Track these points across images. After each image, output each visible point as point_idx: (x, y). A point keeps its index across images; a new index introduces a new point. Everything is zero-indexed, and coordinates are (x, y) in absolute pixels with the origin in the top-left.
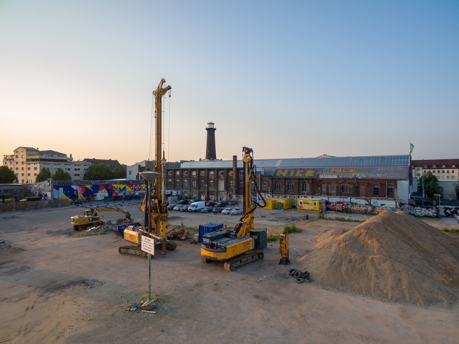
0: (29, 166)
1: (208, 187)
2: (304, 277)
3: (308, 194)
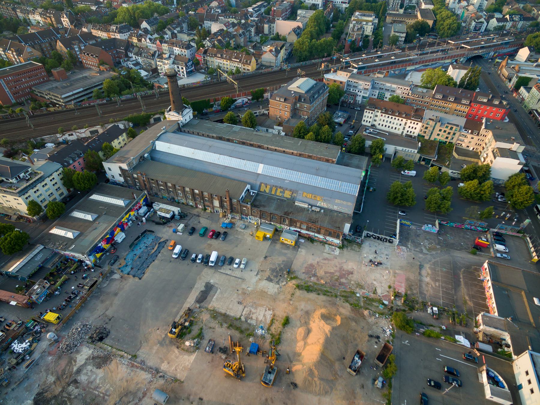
2: (295, 385)
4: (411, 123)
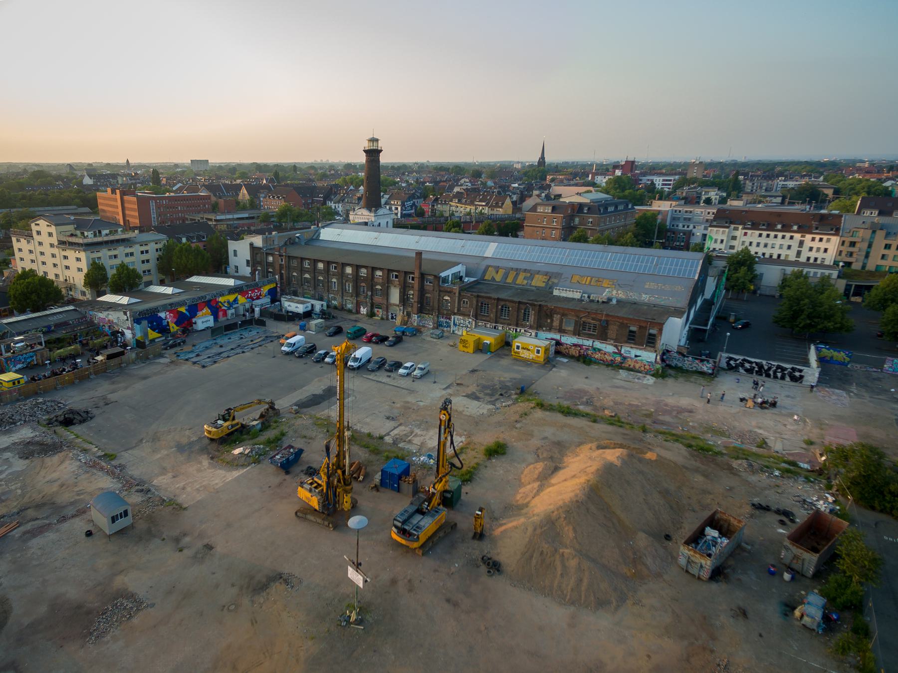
0: (65, 253)
1: (372, 295)
2: (494, 567)
3: (531, 327)
4: (813, 239)
